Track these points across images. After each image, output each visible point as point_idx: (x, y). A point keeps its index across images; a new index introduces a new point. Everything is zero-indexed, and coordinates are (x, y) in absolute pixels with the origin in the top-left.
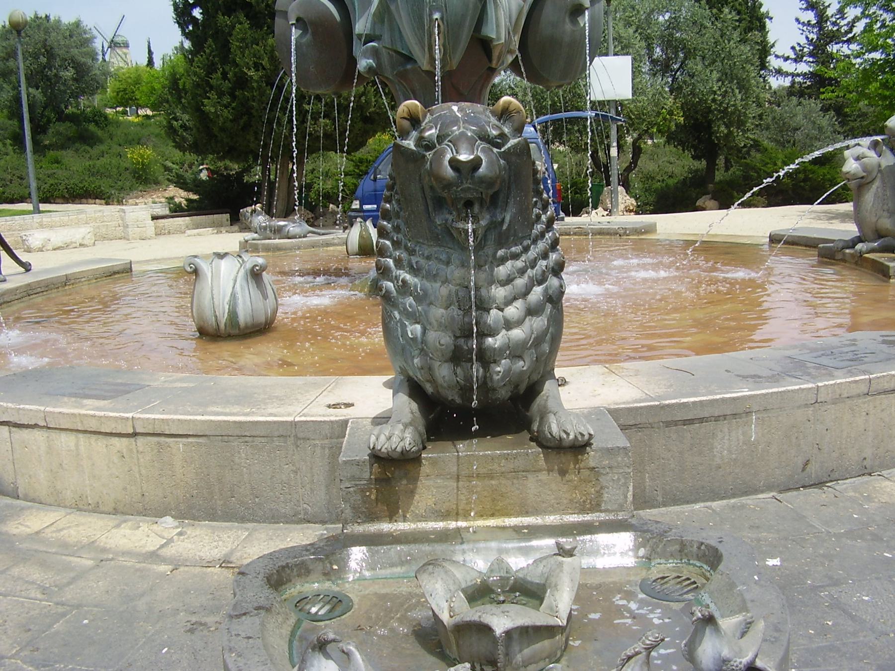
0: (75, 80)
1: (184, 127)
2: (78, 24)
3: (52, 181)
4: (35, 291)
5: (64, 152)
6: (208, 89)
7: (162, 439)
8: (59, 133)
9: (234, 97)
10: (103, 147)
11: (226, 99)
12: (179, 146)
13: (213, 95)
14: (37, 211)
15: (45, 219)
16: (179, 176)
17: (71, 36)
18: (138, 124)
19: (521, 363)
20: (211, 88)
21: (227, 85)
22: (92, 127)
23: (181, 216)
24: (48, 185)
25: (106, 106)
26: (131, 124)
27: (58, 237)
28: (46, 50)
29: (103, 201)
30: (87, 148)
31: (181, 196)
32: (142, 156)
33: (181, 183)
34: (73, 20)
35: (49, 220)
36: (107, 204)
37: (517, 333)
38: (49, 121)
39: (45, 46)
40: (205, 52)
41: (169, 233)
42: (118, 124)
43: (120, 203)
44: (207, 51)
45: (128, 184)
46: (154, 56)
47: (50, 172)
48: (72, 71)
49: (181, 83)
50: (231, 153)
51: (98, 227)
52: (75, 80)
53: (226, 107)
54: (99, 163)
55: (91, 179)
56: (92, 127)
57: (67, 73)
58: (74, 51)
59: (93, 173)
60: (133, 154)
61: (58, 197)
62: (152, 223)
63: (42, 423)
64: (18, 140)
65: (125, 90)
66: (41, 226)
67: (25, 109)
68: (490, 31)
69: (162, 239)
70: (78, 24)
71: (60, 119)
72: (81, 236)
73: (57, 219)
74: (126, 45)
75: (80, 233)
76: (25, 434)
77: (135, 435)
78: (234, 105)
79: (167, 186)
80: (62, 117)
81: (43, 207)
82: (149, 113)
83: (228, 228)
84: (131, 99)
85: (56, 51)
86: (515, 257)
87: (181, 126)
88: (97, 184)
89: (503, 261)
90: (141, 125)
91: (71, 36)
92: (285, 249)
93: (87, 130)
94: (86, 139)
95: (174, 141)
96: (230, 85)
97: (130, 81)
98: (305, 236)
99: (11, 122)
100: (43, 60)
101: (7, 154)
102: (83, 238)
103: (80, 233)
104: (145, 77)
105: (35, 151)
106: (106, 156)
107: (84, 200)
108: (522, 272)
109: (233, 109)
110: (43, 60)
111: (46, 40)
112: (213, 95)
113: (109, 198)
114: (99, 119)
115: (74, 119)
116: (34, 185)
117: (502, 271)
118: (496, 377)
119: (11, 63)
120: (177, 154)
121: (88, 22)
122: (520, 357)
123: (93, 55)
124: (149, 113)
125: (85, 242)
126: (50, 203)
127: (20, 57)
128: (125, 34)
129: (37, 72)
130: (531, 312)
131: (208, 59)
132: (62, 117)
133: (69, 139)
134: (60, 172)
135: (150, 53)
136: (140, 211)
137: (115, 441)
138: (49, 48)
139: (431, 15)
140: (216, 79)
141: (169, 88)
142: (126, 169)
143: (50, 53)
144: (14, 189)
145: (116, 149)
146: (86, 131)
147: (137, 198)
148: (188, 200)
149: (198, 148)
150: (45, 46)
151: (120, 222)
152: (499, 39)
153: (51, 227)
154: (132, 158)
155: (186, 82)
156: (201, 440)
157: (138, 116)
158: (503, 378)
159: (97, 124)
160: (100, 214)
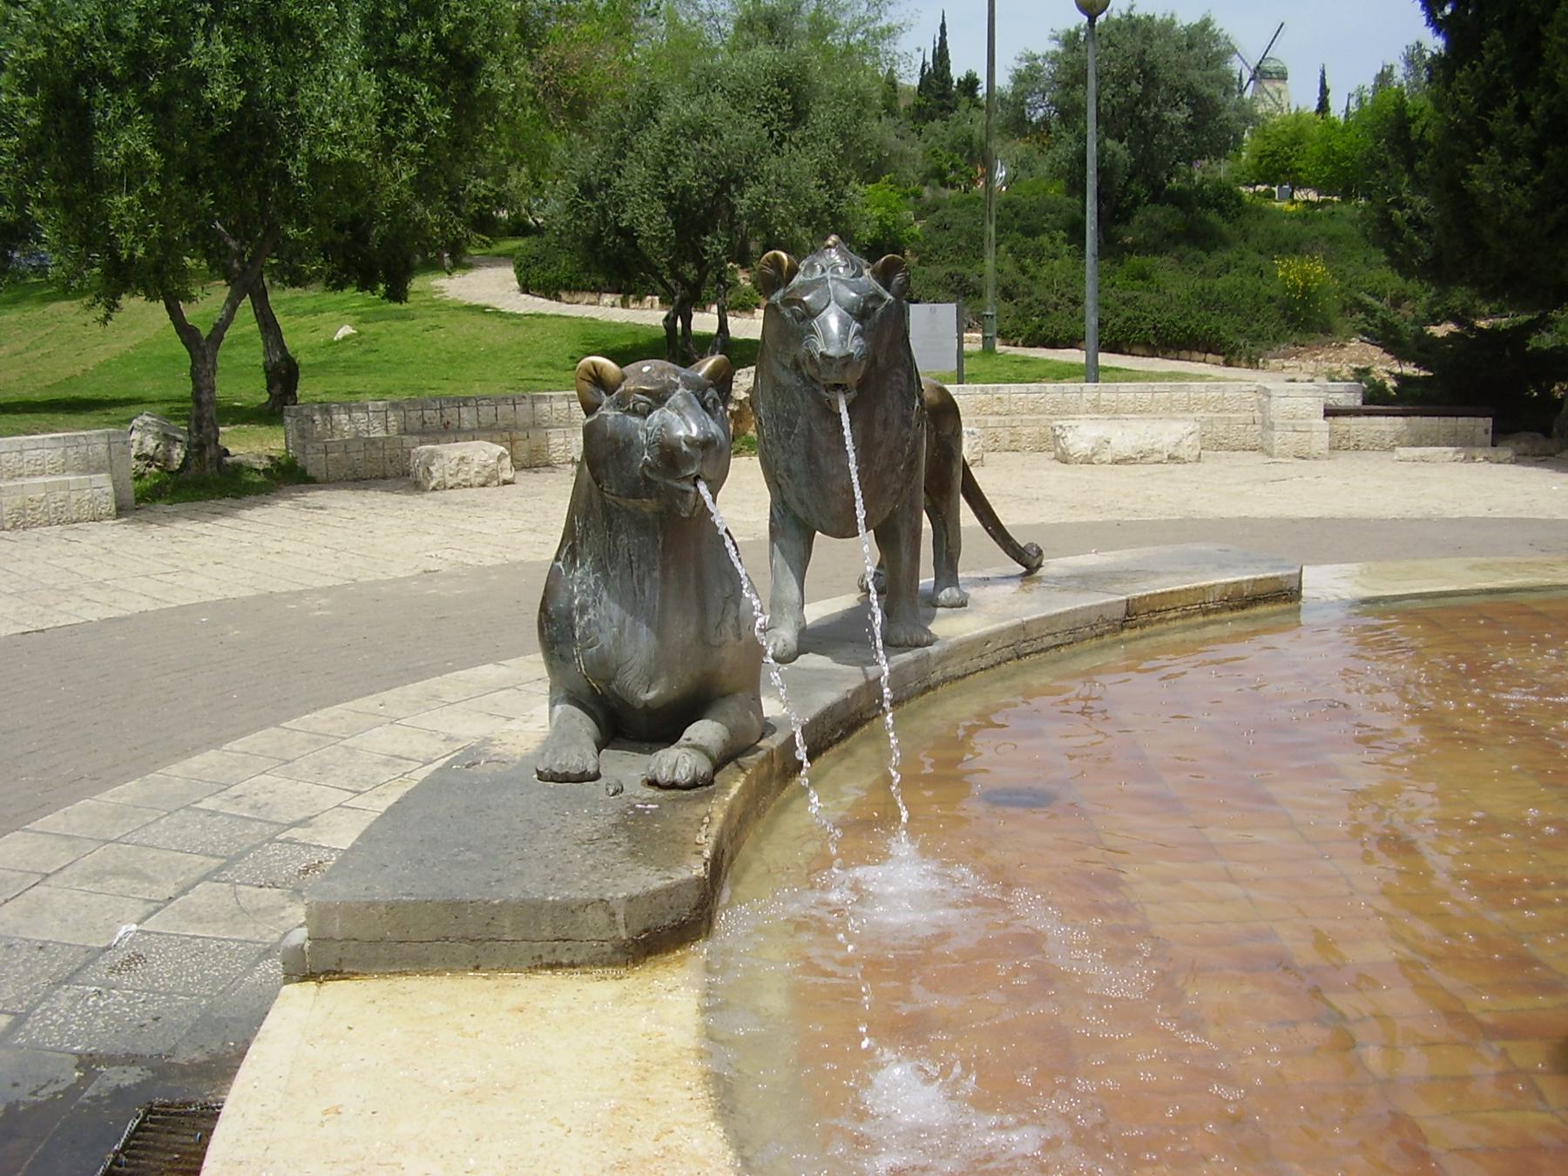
1: (1415, 222)
2: (1205, 25)
3: (1128, 313)
4: (1038, 645)
5: (1157, 260)
6: (1480, 141)
8: (1151, 224)
9: (1539, 162)
10: (1228, 255)
11: (1523, 166)
12: (1401, 265)
13: (1494, 156)
14: (1093, 373)
15: (1104, 392)
16: (1387, 327)
17: (1190, 47)
18: (1292, 217)
20: (1489, 138)
21: (1526, 132)
22: (1212, 216)
23: (1387, 414)
24: (1122, 319)
25: (1237, 180)
26: (1283, 215)
27: (1125, 436)
29: (1221, 359)
31: (1386, 368)
32: (1305, 276)
33: (1390, 340)
34: (1196, 20)
35: (1114, 397)
36: (1228, 364)
38: (1136, 202)
39: (1141, 63)
40: (1481, 58)
41: (1357, 447)
42: (1261, 213)
43: (1252, 363)
44: (1488, 57)
45: (1272, 328)
46: (1330, 96)
47: (1127, 294)
48: (1188, 111)
49: (1415, 129)
50: (1508, 285)
51: (1211, 422)
53: (1520, 184)
54: (1220, 284)
55: (1203, 313)
56: (1212, 216)
58: (1194, 75)
59: (1208, 302)
60: (1289, 271)
61: (1138, 344)
62: (1322, 424)
64: (1076, 231)
65: (1273, 154)
66: (1096, 407)
67: (1091, 172)
69: (1343, 459)
70: (1205, 25)
71: (1153, 200)
72: (1174, 439)
73: (1130, 396)
74: (1282, 76)
75: (1171, 433)
78: (1539, 179)
79: (1348, 338)
80: (1159, 194)
81: (1105, 359)
82: (1313, 196)
83: (1490, 451)
84: (1284, 172)
85: (1162, 73)
87: (1410, 221)
88: (1213, 324)
90: (1304, 218)
91: (1190, 47)
94: (1199, 238)
95: (1390, 252)
96: (1534, 135)
97: (1284, 138)
99: (1069, 200)
100: (1136, 88)
101: (1055, 257)
102: (1178, 444)
103: (1171, 433)
104: (1315, 131)
105: (1102, 254)
106: (1233, 271)
107: (1184, 353)
109: (1536, 187)
110: (1136, 88)
111: (1144, 52)
112: (1494, 156)
113: (1232, 352)
114: (1224, 200)
115: (1180, 200)
116: (1091, 321)
119: (1078, 94)
120: (1394, 282)
121: (1224, 24)
123: (1229, 84)
124: (1313, 196)
125: (1181, 453)
126: (1122, 353)
127: (1092, 84)
128: (1283, 55)
131: (1487, 74)
132: (1159, 194)
133: (1169, 235)
134: (1147, 296)
135: (1324, 91)
136: (1295, 390)
140: (1502, 120)
141: (1388, 140)
142: (1271, 299)
143: (1149, 76)
144: (1058, 323)
145: (1253, 259)
146: (1202, 223)
147: (1286, 357)
148: (1399, 378)
149: (1439, 272)
150: (1141, 63)
151: (1257, 414)
153: (1115, 413)
154: (1285, 279)
155: (1428, 124)
157: (1294, 202)
159: (1221, 210)
160: (1217, 394)
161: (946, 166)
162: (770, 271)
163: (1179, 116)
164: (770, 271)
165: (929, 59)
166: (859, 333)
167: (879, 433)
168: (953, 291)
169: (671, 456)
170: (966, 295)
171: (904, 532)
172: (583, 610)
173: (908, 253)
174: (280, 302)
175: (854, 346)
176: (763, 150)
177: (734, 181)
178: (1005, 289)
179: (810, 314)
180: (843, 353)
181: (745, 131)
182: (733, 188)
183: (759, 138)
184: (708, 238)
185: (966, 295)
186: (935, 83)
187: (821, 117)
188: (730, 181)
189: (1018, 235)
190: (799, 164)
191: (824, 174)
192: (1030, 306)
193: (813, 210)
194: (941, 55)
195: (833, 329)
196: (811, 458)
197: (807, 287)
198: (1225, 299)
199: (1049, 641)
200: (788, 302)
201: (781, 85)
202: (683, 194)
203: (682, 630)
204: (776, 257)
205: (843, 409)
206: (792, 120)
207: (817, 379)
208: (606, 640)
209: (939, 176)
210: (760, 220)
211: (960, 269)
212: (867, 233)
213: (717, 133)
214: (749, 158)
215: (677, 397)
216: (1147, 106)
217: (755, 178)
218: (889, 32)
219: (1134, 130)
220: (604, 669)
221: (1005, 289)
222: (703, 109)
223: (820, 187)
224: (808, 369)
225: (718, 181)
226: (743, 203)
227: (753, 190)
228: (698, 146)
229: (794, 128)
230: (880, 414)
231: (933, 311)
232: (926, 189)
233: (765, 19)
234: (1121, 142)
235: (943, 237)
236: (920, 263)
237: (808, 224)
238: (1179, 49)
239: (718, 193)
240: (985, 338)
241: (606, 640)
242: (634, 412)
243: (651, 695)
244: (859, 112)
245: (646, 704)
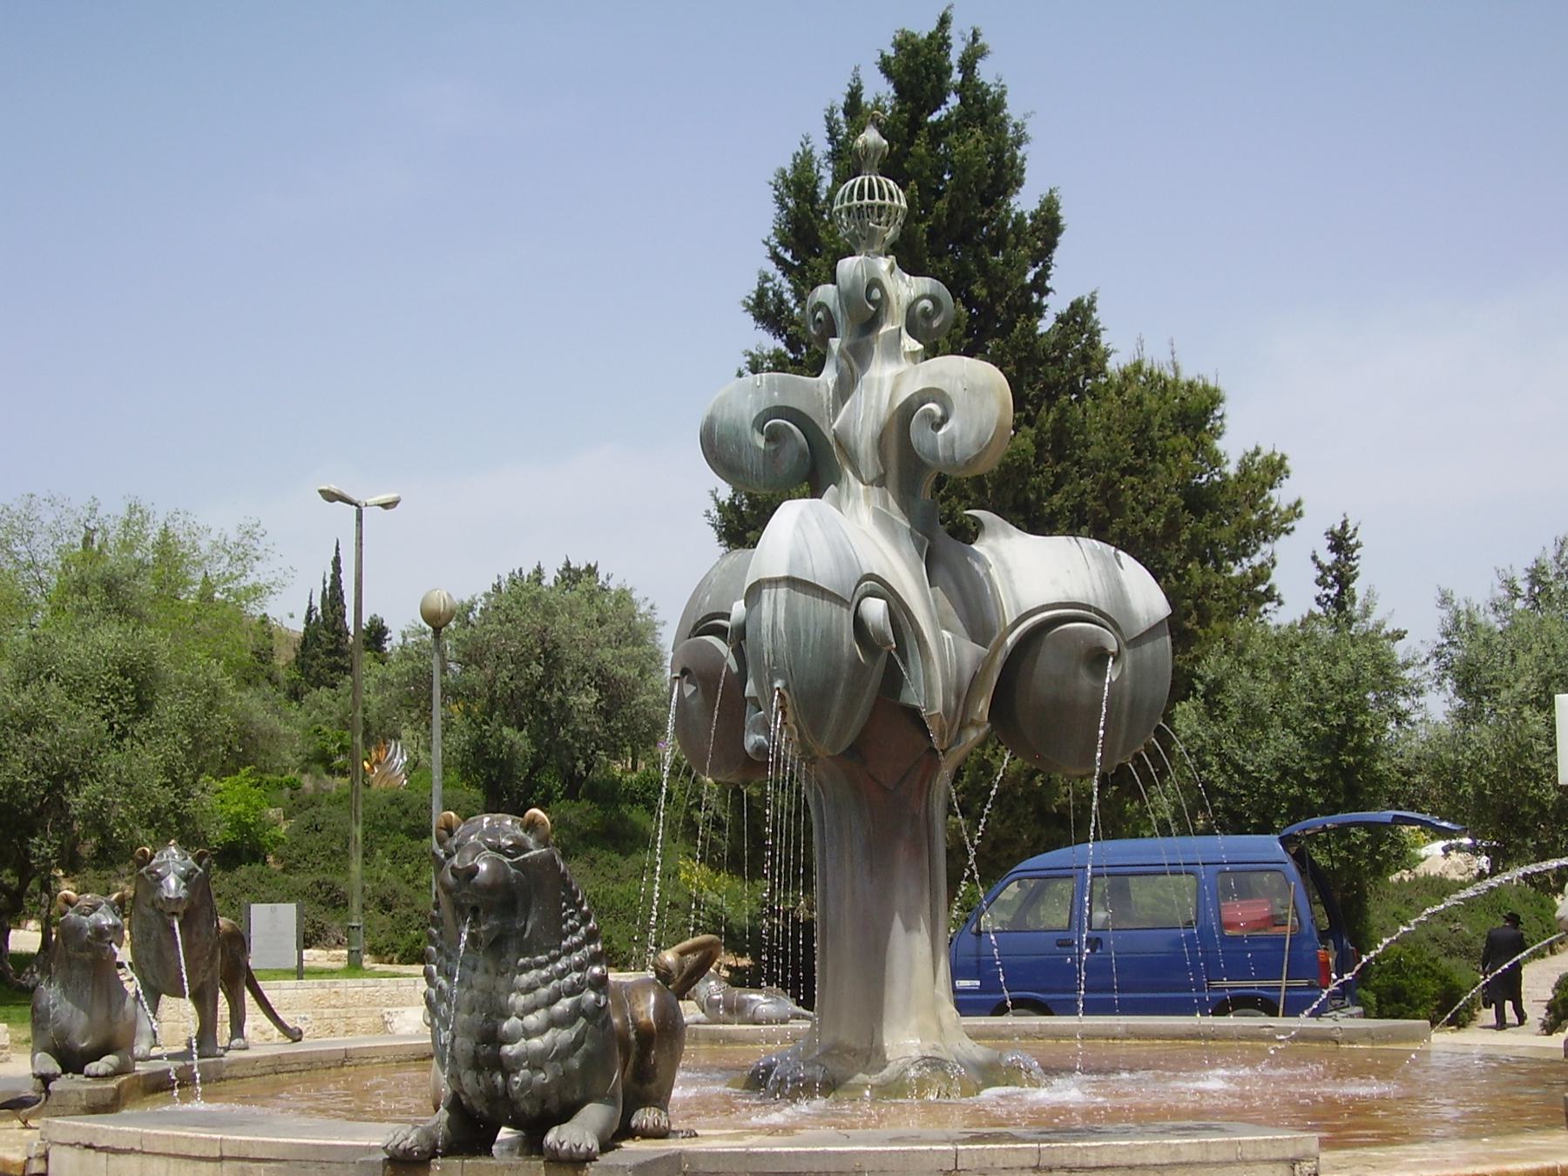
0: (600, 711)
7: (246, 1164)
19: (542, 1075)
28: (544, 651)
30: (615, 857)
37: (536, 1043)
48: (595, 694)
52: (600, 711)
57: (584, 699)
63: (138, 1148)
68: (912, 696)
76: (121, 1161)
77: (222, 1159)
86: (541, 966)
89: (526, 969)
91: (601, 623)
92: (744, 1042)
93: (623, 819)
98: (784, 1021)
100: (538, 670)
108: (546, 981)
110: (538, 670)
117: (525, 979)
118: (516, 1088)
122: (541, 1069)
129: (523, 696)
130: (553, 1023)
137: (203, 1165)
138: (549, 646)
139: (771, 683)
143: (551, 658)
152: (932, 707)
156: (281, 1165)
158: (522, 1090)
161: (333, 748)
163: (586, 700)
165: (317, 603)
168: (320, 902)
169: (100, 932)
170: (335, 907)
171: (209, 993)
172: (54, 1006)
173: (270, 859)
175: (182, 893)
176: (102, 744)
177: (68, 778)
178: (383, 900)
179: (160, 878)
181: (81, 724)
182: (67, 785)
183: (98, 731)
184: (37, 840)
185: (335, 907)
186: (325, 635)
187: (168, 709)
188: (63, 778)
189: (402, 837)
190: (144, 762)
191: (169, 771)
192: (408, 918)
193: (157, 810)
194: (334, 597)
195: (172, 886)
196: (159, 952)
197: (159, 865)
198: (620, 906)
199: (295, 1067)
200: (149, 872)
201: (124, 674)
202: (10, 792)
203: (100, 1014)
205: (176, 924)
206: (135, 711)
207: (164, 910)
208: (64, 1020)
209: (324, 759)
210: (97, 821)
211: (329, 877)
212: (219, 834)
213: (50, 725)
214: (85, 754)
215: (102, 908)
216: (550, 689)
217: (92, 775)
218: (256, 591)
219: (535, 717)
220: (63, 1034)
221: (383, 900)
222: (35, 699)
223: (165, 785)
224: (159, 905)
225: (48, 777)
226: (78, 802)
227: (90, 788)
228: (28, 739)
229: (137, 719)
230: (195, 929)
231: (273, 911)
232: (306, 777)
233: (102, 581)
234: (520, 730)
235: (311, 840)
236: (284, 870)
237: (150, 825)
238: (588, 625)
239: (48, 790)
240: (351, 952)
241: (64, 1020)
244: (210, 706)
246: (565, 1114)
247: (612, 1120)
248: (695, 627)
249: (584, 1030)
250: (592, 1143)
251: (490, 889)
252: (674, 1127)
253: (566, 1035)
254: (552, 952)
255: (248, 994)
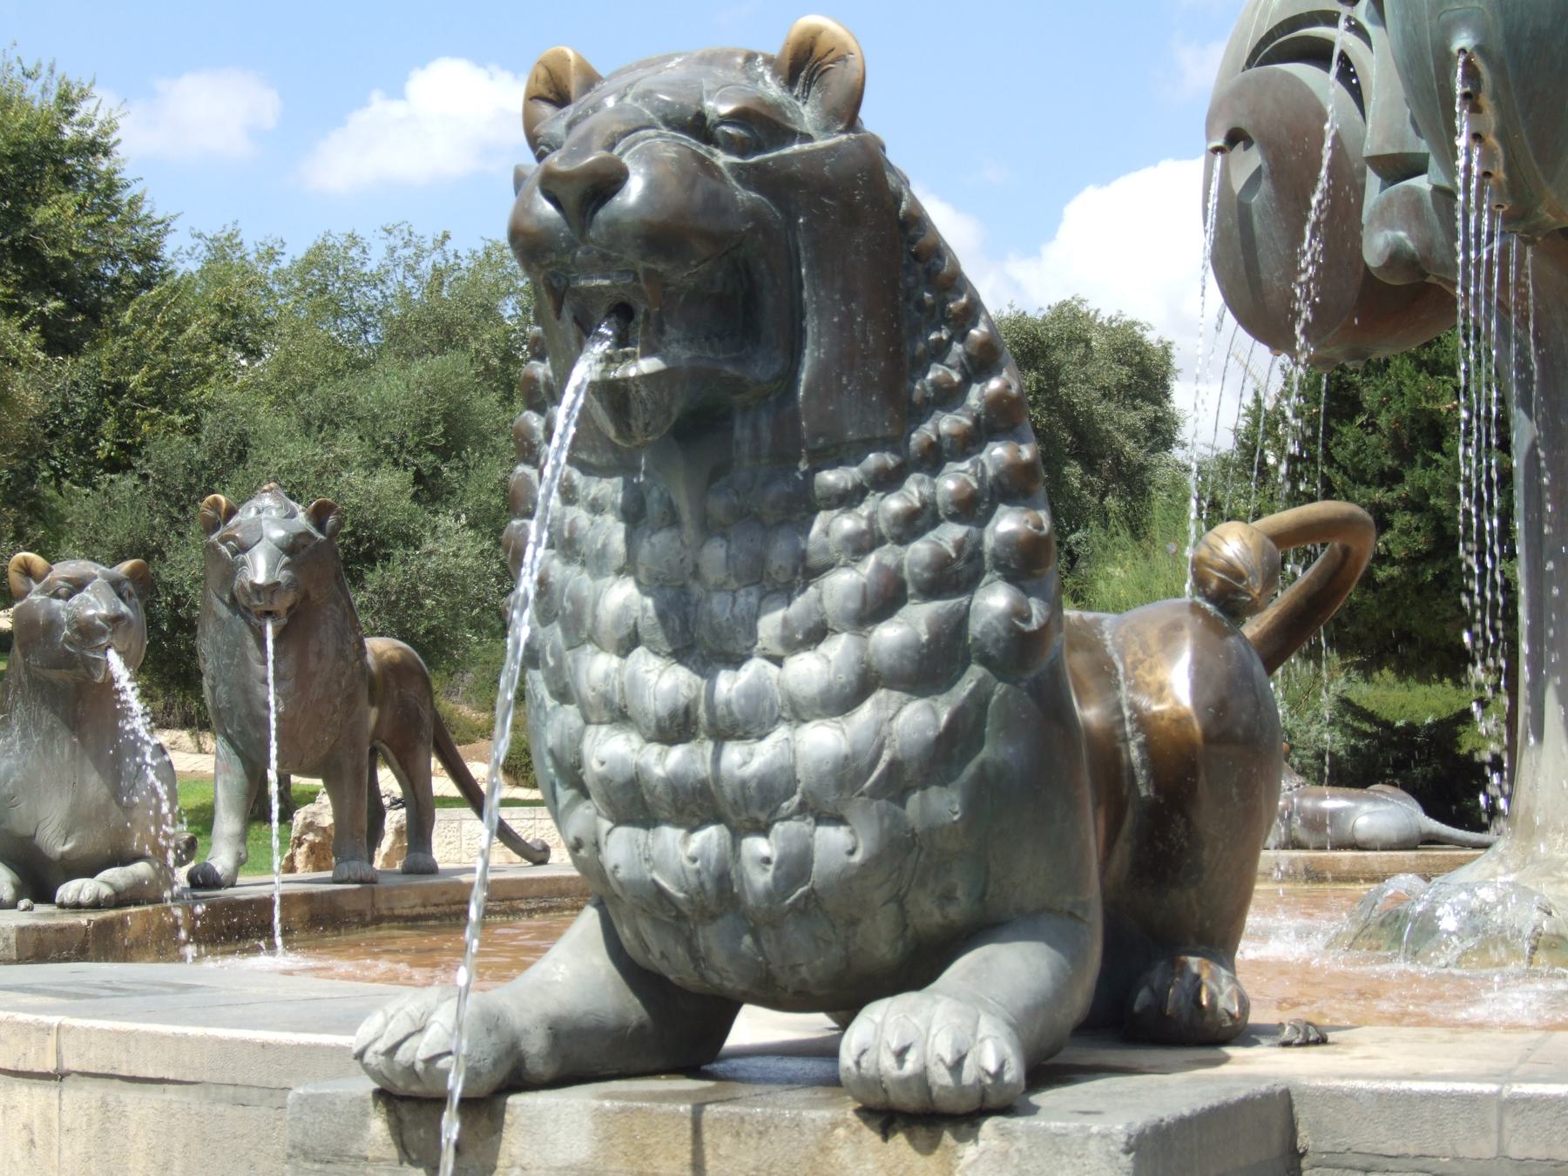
2: (885, 1138)
70: (885, 1138)
162: (211, 513)
164: (211, 513)
166: (286, 566)
167: (313, 664)
174: (889, 697)
180: (271, 581)
204: (216, 500)
242: (56, 595)
243: (67, 847)
245: (63, 856)
246: (917, 967)
247: (1060, 992)
248: (1264, 41)
249: (979, 699)
250: (995, 1054)
251: (661, 237)
252: (1255, 1018)
253: (914, 719)
254: (873, 460)
255: (435, 764)
